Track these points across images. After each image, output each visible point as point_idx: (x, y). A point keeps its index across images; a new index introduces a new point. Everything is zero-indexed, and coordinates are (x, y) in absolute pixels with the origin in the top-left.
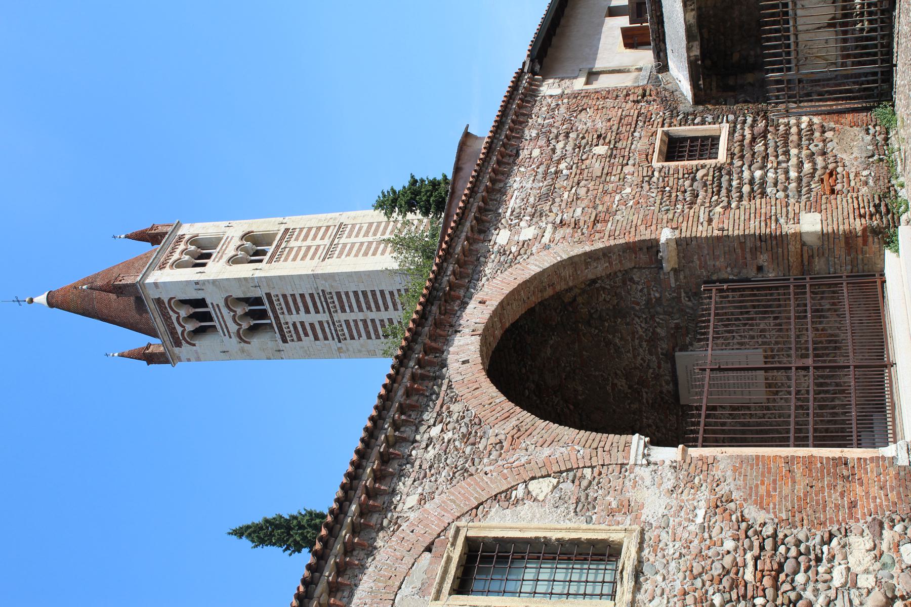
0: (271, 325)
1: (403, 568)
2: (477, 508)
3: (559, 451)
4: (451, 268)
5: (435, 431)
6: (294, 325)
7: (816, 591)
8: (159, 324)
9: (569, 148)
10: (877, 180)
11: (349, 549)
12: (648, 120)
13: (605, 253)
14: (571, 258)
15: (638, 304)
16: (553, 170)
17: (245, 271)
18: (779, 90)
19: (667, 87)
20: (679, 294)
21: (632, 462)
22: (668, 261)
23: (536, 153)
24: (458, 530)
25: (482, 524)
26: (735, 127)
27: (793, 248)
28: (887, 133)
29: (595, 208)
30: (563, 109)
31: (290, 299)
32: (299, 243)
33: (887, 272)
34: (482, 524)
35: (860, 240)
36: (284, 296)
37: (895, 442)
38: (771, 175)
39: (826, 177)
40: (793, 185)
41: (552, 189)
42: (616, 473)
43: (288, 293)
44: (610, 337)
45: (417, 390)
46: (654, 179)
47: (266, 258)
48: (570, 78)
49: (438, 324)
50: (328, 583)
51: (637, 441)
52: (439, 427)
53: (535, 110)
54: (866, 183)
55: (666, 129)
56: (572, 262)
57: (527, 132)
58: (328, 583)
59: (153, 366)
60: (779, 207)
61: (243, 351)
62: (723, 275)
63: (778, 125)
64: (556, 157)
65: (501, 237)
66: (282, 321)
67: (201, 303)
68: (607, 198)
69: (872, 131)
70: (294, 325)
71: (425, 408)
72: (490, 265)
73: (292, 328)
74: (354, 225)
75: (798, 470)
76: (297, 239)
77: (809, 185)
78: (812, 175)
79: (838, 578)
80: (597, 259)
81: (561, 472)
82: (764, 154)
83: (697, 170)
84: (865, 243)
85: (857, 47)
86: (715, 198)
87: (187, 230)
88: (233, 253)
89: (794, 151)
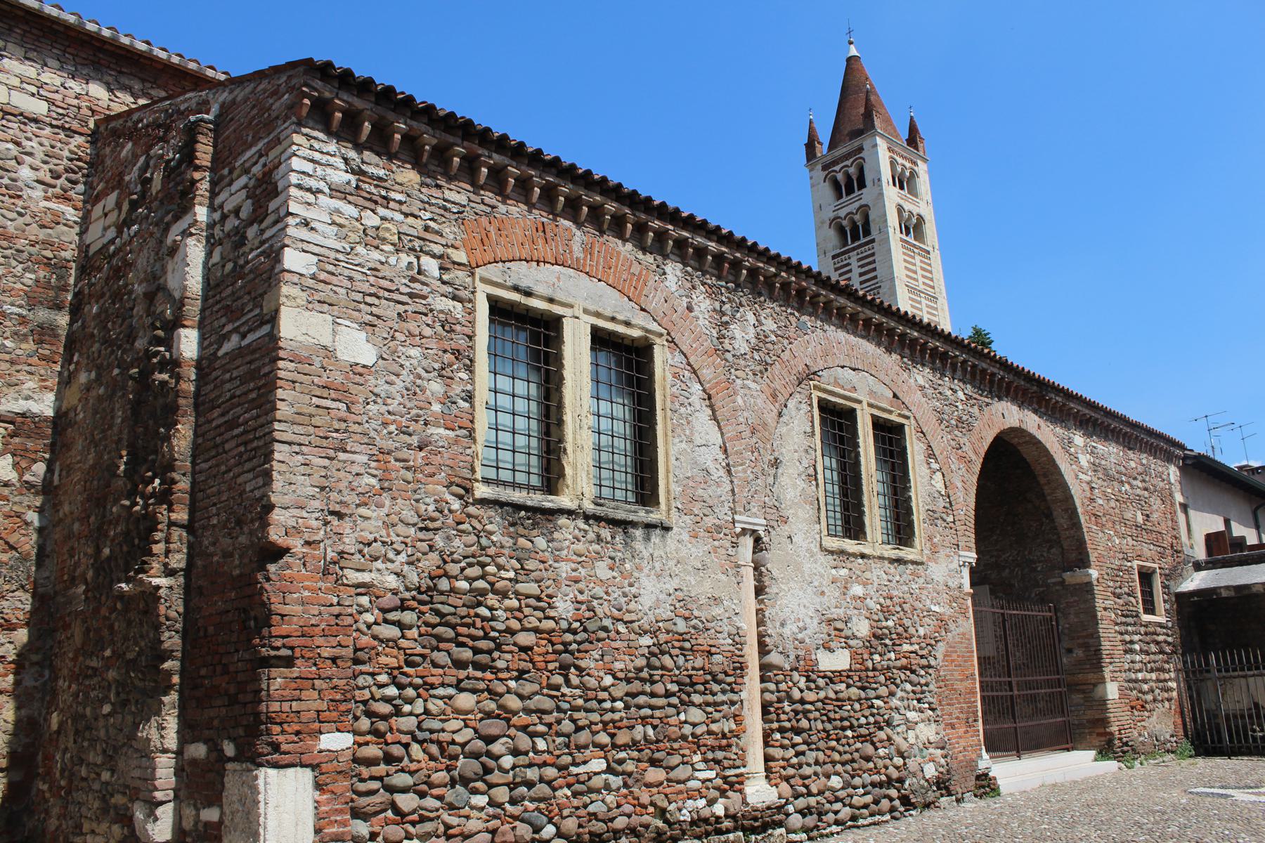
0: (845, 244)
1: (882, 377)
2: (922, 432)
3: (961, 494)
4: (1060, 400)
5: (960, 394)
6: (848, 264)
7: (902, 699)
8: (840, 151)
9: (1138, 491)
10: (1143, 743)
11: (891, 332)
12: (1162, 555)
13: (1076, 525)
14: (1072, 497)
15: (1030, 553)
16: (1124, 479)
17: (893, 220)
18: (1193, 663)
20: (1042, 586)
21: (961, 553)
22: (1072, 576)
23: (1133, 464)
24: (907, 418)
25: (914, 440)
26: (1164, 628)
27: (1091, 677)
28: (1173, 752)
29: (1104, 515)
30: (1161, 484)
31: (871, 259)
32: (919, 264)
33: (1075, 752)
34: (914, 440)
35: (1102, 730)
36: (873, 254)
37: (991, 758)
38: (1138, 658)
39: (1140, 702)
40: (1133, 676)
41: (1112, 479)
42: (953, 541)
43: (876, 257)
44: (998, 532)
45: (985, 379)
46: (1126, 563)
47: (904, 237)
48: (1181, 489)
49: (1025, 392)
50: (871, 318)
51: (972, 556)
52: (963, 398)
53: (1159, 462)
55: (1158, 571)
56: (1069, 498)
57: (1145, 455)
58: (871, 318)
59: (804, 148)
61: (823, 222)
62: (1061, 622)
63: (1168, 662)
64: (1131, 480)
65: (1079, 439)
66: (851, 254)
67: (862, 185)
68: (1110, 524)
69: (1173, 739)
70: (848, 264)
71: (974, 387)
72: (1061, 431)
73: (845, 262)
74: (936, 309)
75: (968, 683)
76: (921, 261)
77: (1135, 689)
78: (1140, 691)
79: (912, 715)
80: (1071, 518)
81: (949, 497)
84: (1099, 735)
85: (1237, 727)
86: (1120, 613)
87: (922, 168)
88: (906, 208)
89: (1154, 676)
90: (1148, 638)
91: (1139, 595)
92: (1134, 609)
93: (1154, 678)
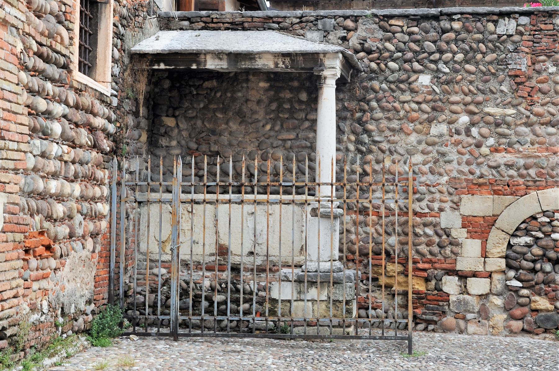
19: (147, 21)
38: (55, 149)
40: (41, 185)
54: (33, 309)
60: (16, 155)
78: (49, 218)
82: (77, 142)
83: (68, 29)
86: (35, 47)
89: (77, 189)
90: (79, 116)
91: (76, 28)
92: (64, 51)
93: (77, 193)
